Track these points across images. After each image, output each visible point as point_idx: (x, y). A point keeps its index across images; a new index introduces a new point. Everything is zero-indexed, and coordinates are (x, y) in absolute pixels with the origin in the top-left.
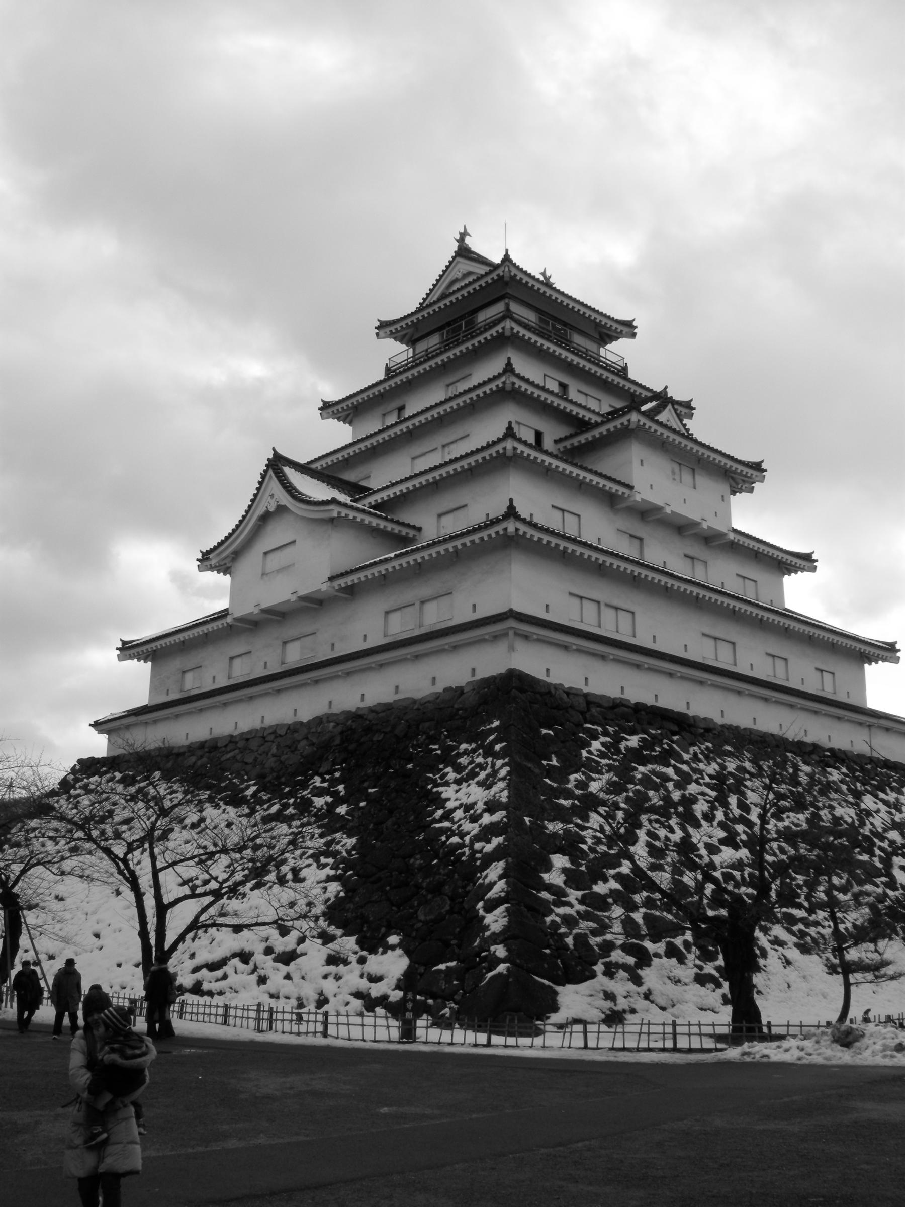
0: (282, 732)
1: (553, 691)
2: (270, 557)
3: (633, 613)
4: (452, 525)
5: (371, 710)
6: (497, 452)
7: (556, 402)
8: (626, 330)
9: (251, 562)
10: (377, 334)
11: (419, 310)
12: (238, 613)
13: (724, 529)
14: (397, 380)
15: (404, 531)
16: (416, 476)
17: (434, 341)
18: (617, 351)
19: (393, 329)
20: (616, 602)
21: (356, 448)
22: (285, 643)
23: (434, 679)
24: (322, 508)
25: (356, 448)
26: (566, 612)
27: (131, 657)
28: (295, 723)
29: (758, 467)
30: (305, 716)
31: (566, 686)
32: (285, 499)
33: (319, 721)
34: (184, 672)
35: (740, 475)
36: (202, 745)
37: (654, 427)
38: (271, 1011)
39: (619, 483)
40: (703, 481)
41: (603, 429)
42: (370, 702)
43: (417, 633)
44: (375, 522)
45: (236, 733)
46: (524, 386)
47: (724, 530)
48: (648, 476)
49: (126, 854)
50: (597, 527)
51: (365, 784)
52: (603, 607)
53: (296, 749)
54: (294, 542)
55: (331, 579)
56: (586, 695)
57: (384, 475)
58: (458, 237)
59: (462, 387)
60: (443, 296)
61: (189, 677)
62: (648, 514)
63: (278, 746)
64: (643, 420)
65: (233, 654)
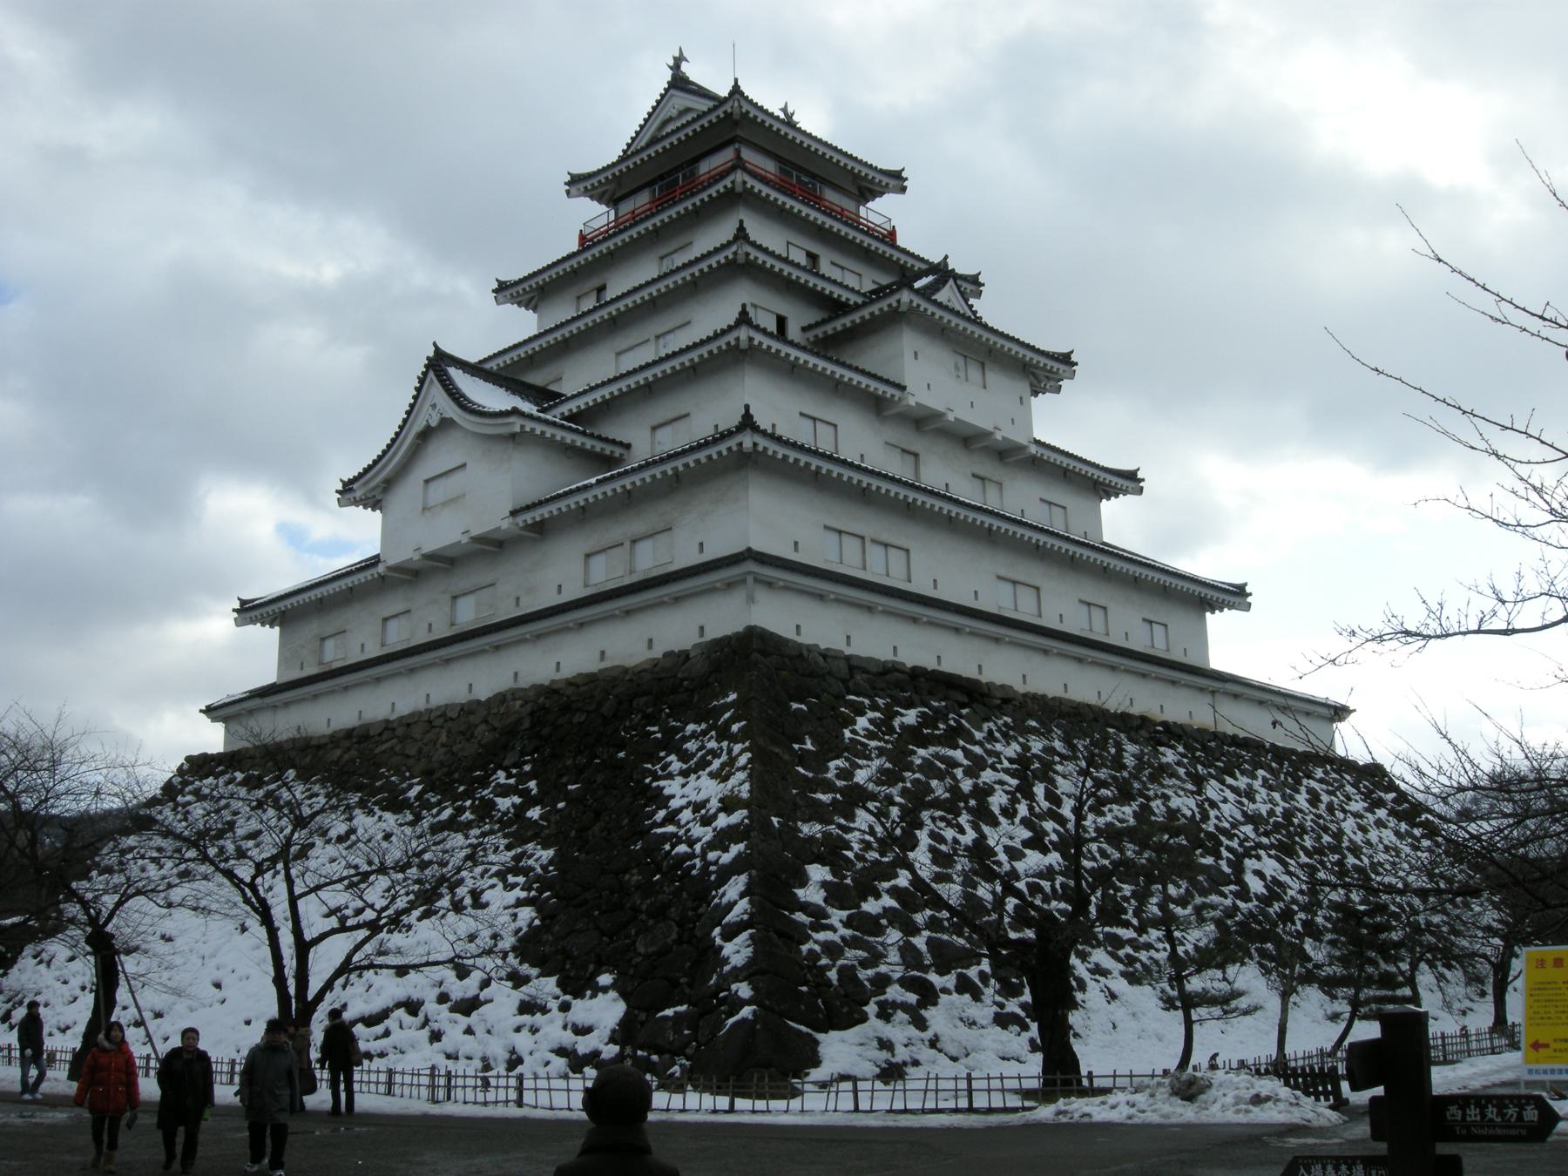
0: (454, 714)
1: (805, 653)
2: (433, 485)
3: (907, 551)
4: (671, 440)
5: (570, 683)
6: (728, 344)
7: (804, 277)
8: (892, 182)
9: (408, 493)
10: (568, 192)
11: (622, 160)
12: (393, 559)
13: (1023, 441)
14: (596, 251)
15: (608, 449)
16: (622, 376)
17: (642, 200)
18: (879, 210)
19: (588, 184)
20: (885, 538)
21: (543, 342)
22: (455, 598)
23: (650, 641)
24: (500, 421)
25: (543, 342)
26: (820, 551)
27: (253, 621)
28: (471, 703)
29: (1066, 359)
30: (483, 692)
31: (823, 647)
32: (451, 410)
33: (502, 698)
34: (323, 639)
35: (1043, 370)
36: (349, 734)
37: (931, 309)
38: (449, 1075)
39: (887, 382)
40: (995, 378)
41: (866, 313)
42: (568, 672)
43: (627, 581)
44: (569, 438)
45: (393, 717)
46: (762, 257)
47: (1024, 442)
48: (924, 373)
49: (254, 878)
50: (859, 440)
51: (564, 780)
52: (868, 544)
53: (472, 736)
54: (464, 466)
55: (514, 513)
56: (848, 658)
57: (580, 377)
58: (671, 63)
59: (680, 259)
60: (654, 141)
61: (329, 644)
62: (924, 422)
63: (449, 732)
64: (917, 300)
65: (387, 614)
